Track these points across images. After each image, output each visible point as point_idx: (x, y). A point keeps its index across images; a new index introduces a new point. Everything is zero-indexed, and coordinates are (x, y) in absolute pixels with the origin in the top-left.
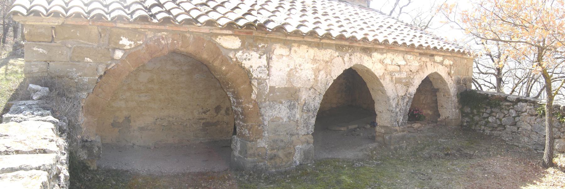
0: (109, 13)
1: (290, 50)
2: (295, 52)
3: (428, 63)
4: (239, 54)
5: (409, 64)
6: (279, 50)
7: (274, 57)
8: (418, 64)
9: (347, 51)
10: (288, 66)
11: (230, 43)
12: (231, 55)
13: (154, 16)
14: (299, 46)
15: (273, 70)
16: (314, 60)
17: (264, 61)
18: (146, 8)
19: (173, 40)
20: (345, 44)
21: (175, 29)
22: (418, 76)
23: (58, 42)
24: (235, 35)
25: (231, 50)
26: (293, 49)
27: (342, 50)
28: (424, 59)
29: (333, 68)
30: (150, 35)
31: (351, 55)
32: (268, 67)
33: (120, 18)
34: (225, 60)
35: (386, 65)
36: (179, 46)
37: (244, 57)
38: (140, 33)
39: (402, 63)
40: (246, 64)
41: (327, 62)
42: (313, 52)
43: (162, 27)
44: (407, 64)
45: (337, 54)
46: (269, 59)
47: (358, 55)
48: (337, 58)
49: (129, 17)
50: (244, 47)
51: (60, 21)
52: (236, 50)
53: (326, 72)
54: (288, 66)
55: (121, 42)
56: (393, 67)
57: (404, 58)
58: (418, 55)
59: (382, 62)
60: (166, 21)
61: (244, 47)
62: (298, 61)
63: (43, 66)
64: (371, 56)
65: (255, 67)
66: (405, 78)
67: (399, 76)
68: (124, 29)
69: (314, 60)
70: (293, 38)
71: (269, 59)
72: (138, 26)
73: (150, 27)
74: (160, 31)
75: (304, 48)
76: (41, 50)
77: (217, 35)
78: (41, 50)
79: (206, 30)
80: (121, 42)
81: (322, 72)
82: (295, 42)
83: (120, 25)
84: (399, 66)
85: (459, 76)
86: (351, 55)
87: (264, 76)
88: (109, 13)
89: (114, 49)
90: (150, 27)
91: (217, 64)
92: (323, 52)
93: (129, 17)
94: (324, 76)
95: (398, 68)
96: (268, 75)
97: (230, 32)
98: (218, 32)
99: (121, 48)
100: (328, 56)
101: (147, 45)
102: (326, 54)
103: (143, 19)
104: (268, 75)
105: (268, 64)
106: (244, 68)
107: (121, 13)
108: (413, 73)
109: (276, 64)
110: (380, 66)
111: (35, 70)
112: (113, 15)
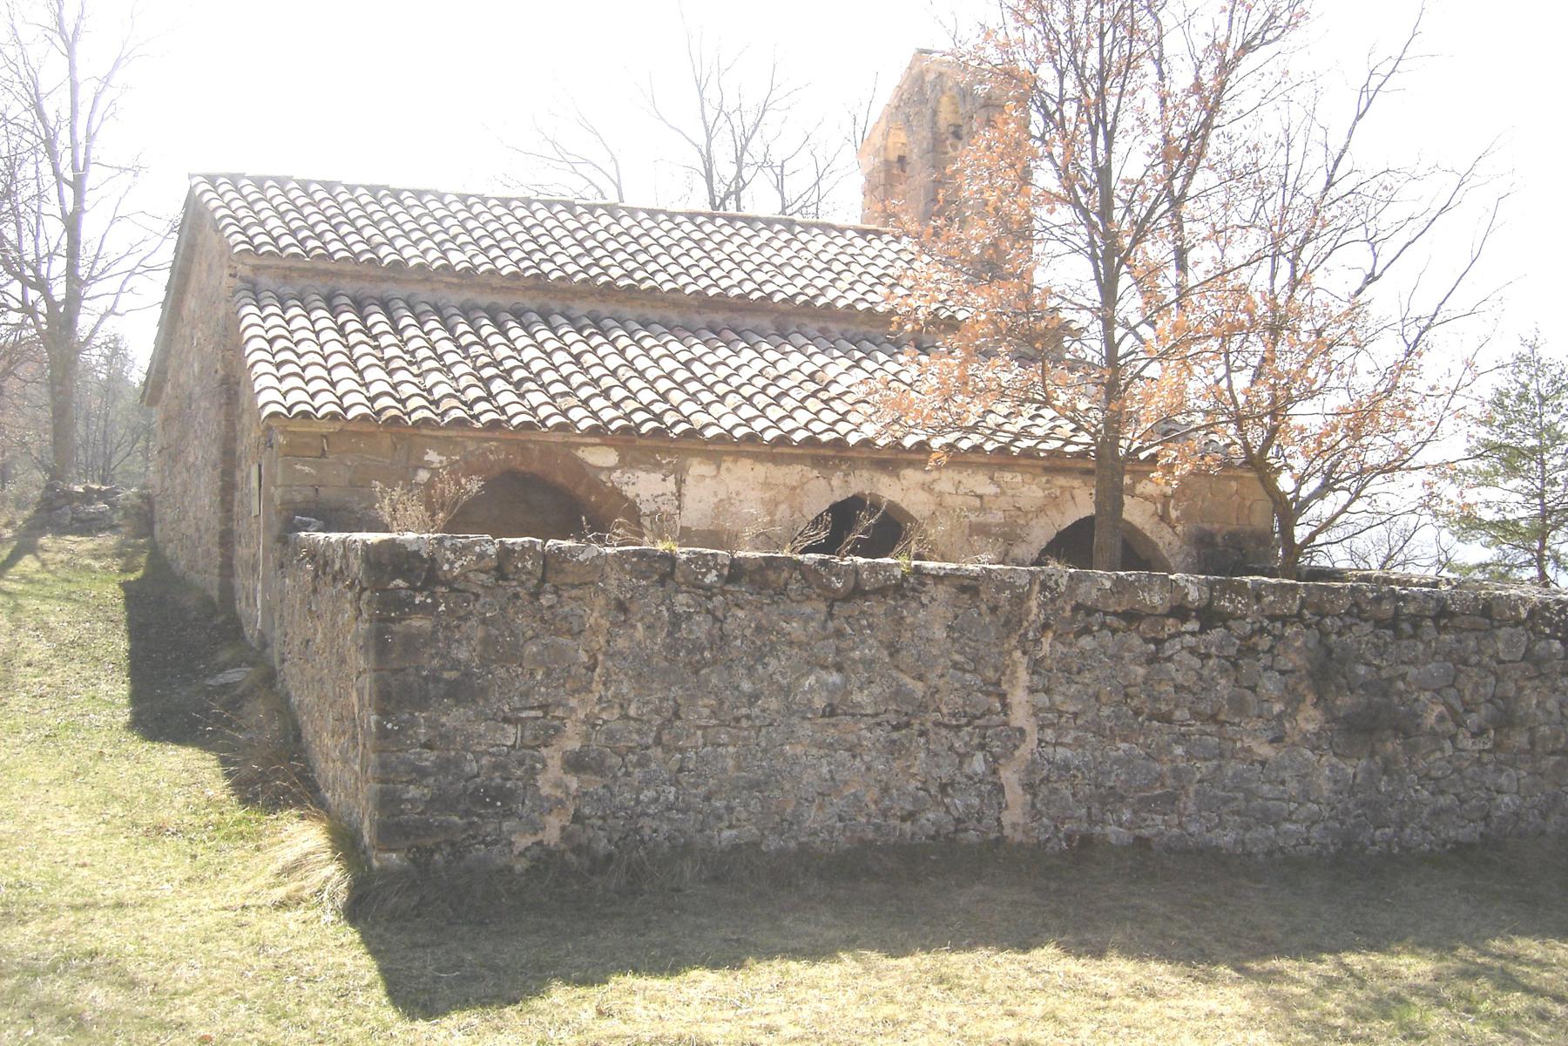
0: (409, 414)
1: (719, 468)
2: (728, 469)
3: (1077, 492)
4: (616, 475)
5: (1010, 492)
6: (698, 468)
7: (689, 480)
8: (1040, 494)
9: (837, 467)
10: (716, 494)
11: (601, 457)
12: (603, 477)
13: (476, 417)
14: (735, 461)
15: (687, 501)
16: (767, 485)
17: (671, 484)
18: (465, 403)
19: (508, 454)
20: (828, 454)
21: (509, 436)
22: (1043, 520)
23: (332, 458)
24: (609, 446)
25: (602, 469)
26: (724, 466)
27: (825, 466)
28: (1062, 481)
29: (806, 499)
30: (471, 446)
31: (846, 475)
32: (679, 495)
33: (426, 420)
34: (596, 486)
35: (941, 494)
36: (517, 462)
37: (625, 479)
38: (456, 443)
39: (991, 490)
40: (630, 491)
41: (794, 488)
42: (762, 470)
43: (489, 435)
44: (1003, 493)
45: (815, 473)
46: (680, 483)
47: (866, 474)
48: (816, 482)
49: (438, 419)
50: (623, 464)
51: (337, 426)
52: (611, 469)
53: (791, 507)
54: (716, 494)
55: (426, 458)
56: (960, 500)
57: (992, 478)
58: (1039, 471)
59: (927, 488)
60: (494, 424)
61: (623, 464)
62: (734, 485)
63: (310, 493)
64: (898, 477)
65: (645, 495)
66: (997, 525)
67: (981, 519)
68: (431, 437)
69: (767, 485)
70: (718, 448)
71: (680, 483)
72: (451, 433)
73: (471, 434)
74: (488, 440)
75: (748, 463)
76: (307, 469)
77: (578, 446)
78: (307, 469)
79: (557, 437)
80: (426, 458)
81: (783, 507)
82: (728, 453)
83: (425, 432)
84: (981, 497)
85: (1207, 526)
86: (846, 475)
87: (670, 509)
88: (409, 414)
89: (416, 468)
90: (471, 434)
91: (580, 491)
92: (785, 469)
93: (438, 419)
94: (787, 514)
95: (977, 502)
96: (679, 507)
97: (598, 440)
98: (578, 440)
99: (426, 466)
100: (797, 477)
101: (466, 462)
102: (791, 474)
103: (459, 422)
104: (679, 507)
105: (679, 490)
106: (626, 499)
107: (427, 413)
108: (1026, 513)
109: (692, 491)
110: (923, 496)
111: (298, 498)
112: (415, 417)
